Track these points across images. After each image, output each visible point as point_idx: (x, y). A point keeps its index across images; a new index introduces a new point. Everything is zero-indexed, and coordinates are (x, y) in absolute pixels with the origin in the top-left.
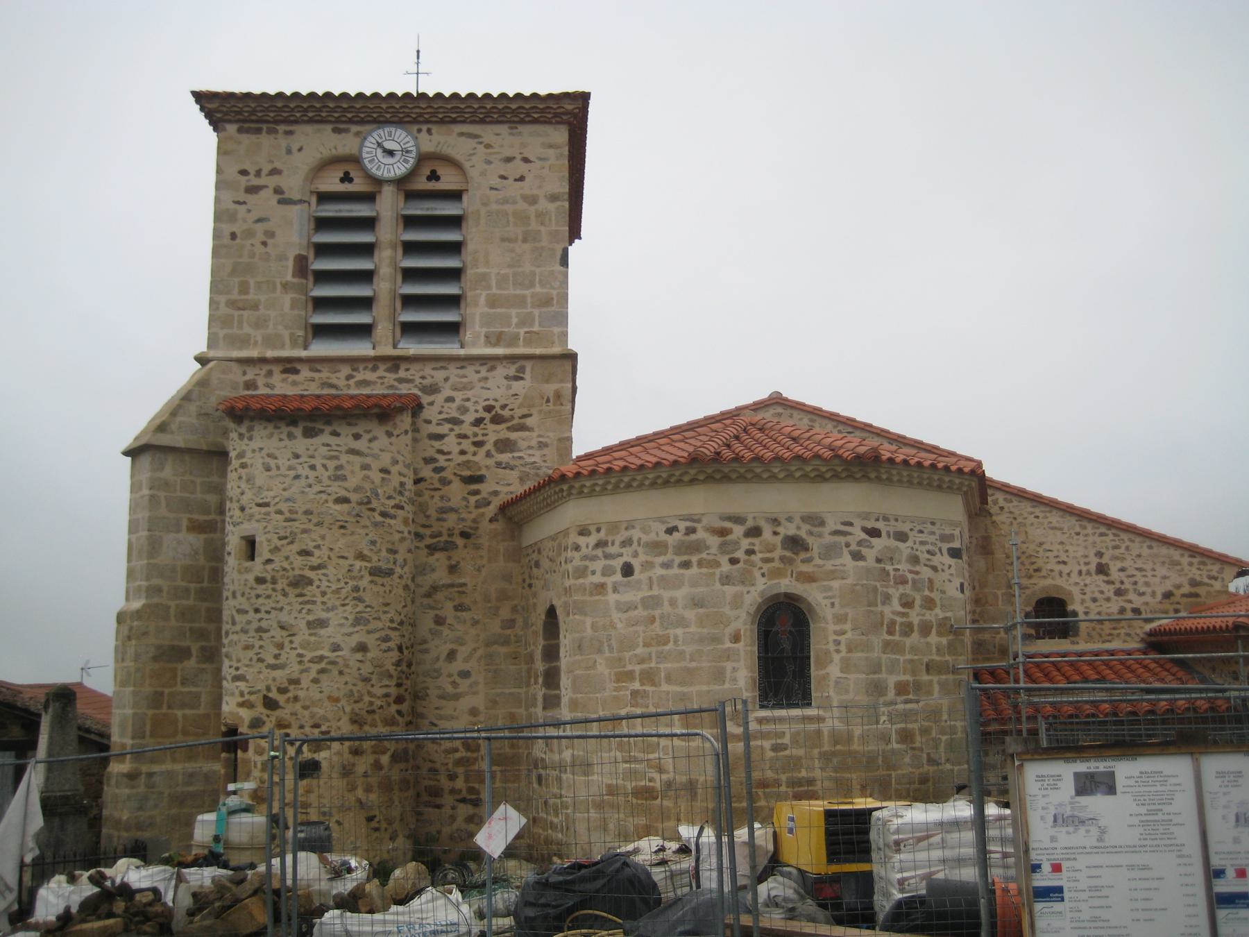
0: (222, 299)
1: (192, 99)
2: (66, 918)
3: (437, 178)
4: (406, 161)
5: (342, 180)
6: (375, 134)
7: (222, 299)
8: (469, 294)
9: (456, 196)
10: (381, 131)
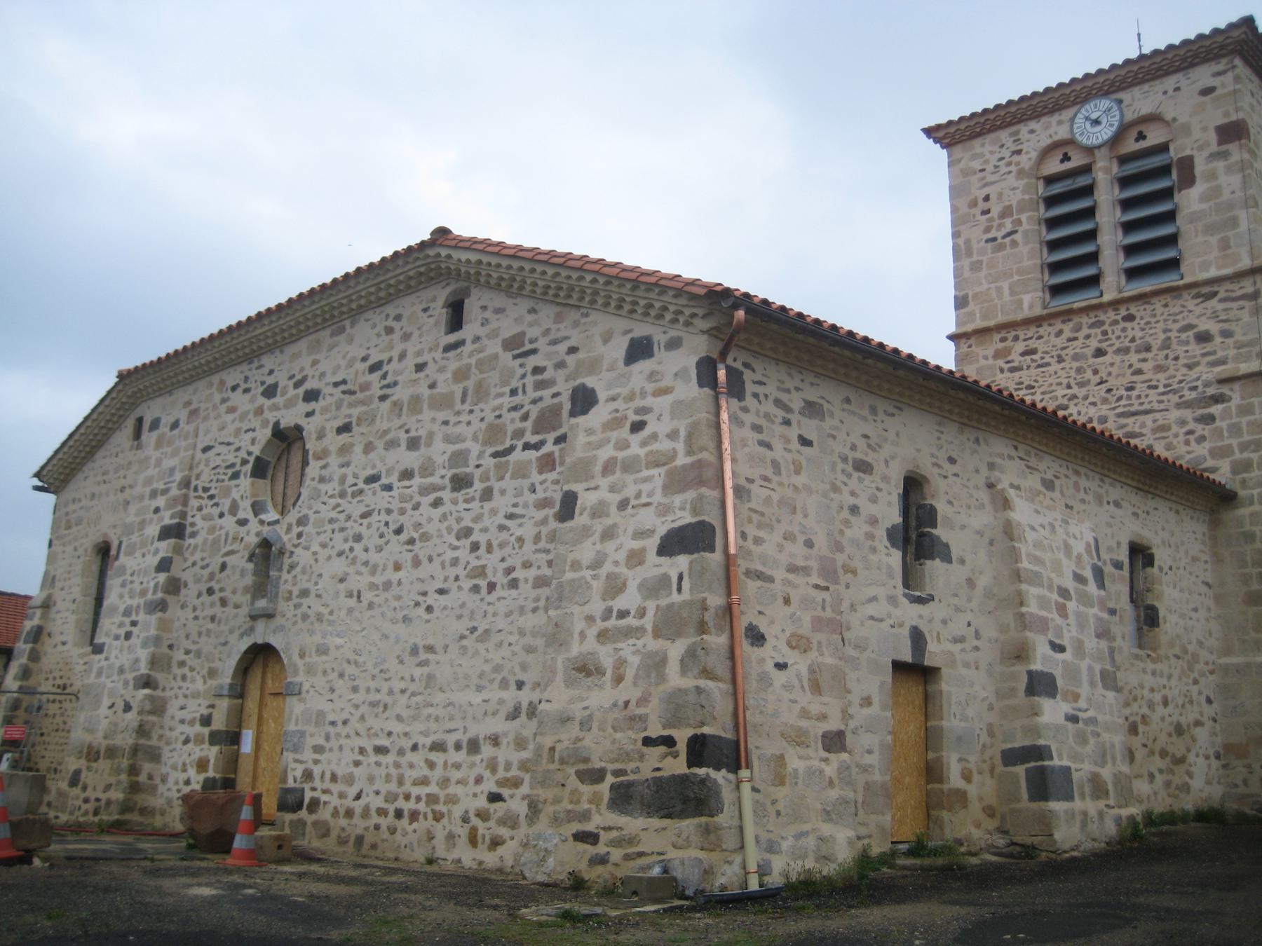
0: (966, 263)
1: (924, 136)
2: (683, 466)
3: (1144, 138)
4: (1112, 125)
5: (1062, 161)
6: (1083, 111)
7: (966, 263)
8: (1183, 229)
9: (1163, 148)
10: (1087, 107)
